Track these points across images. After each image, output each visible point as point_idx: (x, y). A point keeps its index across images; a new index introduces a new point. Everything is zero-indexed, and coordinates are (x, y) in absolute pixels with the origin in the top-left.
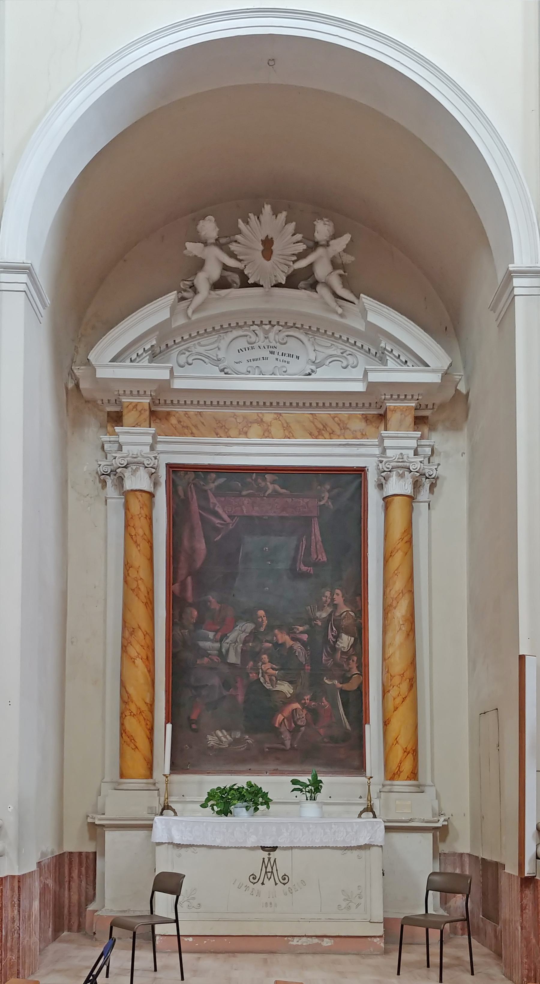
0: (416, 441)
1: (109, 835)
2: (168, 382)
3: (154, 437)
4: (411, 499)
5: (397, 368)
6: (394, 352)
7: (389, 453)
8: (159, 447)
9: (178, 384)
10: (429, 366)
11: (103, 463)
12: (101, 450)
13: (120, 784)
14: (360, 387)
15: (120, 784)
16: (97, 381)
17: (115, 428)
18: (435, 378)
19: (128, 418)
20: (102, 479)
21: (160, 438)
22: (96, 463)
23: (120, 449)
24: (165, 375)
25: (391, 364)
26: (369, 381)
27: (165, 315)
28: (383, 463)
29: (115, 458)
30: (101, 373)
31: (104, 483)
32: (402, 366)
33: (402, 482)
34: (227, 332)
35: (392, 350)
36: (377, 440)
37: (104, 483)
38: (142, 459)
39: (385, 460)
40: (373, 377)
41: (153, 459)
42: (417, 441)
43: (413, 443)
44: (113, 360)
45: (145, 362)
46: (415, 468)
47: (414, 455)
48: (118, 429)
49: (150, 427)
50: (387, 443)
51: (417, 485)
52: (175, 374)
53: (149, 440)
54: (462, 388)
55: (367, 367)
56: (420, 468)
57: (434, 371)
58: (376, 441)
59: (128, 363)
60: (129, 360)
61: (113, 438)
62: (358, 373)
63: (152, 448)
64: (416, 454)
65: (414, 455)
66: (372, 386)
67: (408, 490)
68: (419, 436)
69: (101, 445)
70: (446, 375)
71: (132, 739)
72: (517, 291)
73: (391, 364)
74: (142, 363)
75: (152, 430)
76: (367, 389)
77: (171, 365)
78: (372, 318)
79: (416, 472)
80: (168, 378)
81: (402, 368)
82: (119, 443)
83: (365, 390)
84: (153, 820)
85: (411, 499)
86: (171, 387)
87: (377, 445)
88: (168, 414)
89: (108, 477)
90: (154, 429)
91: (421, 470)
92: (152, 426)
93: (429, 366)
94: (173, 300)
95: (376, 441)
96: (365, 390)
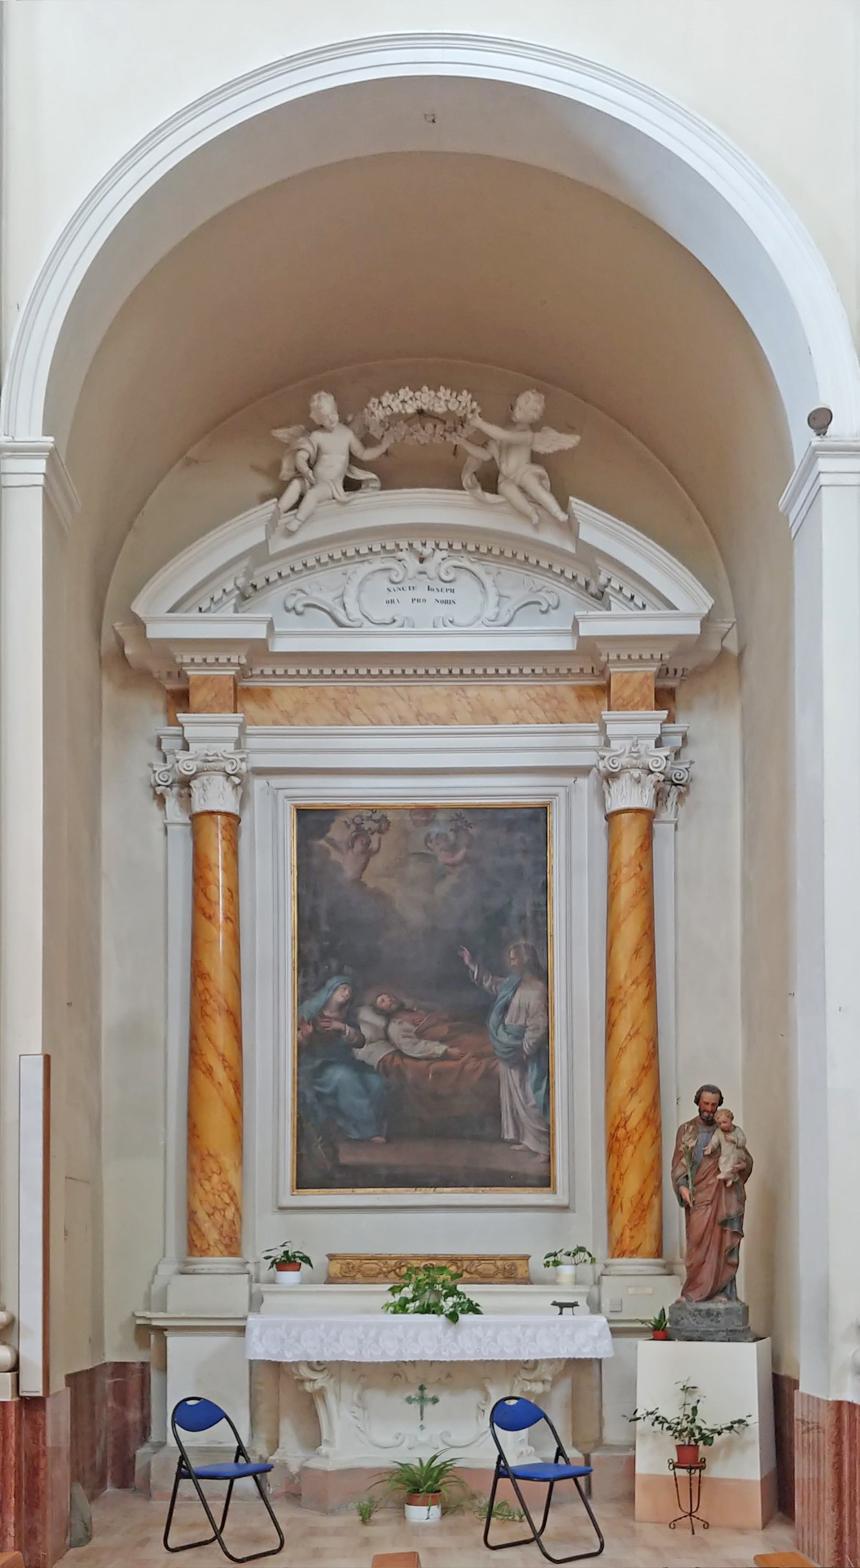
0: (659, 725)
1: (173, 1342)
2: (264, 642)
3: (242, 728)
4: (648, 816)
5: (624, 613)
6: (624, 591)
7: (614, 744)
8: (252, 743)
9: (281, 645)
10: (677, 609)
11: (159, 770)
12: (155, 749)
13: (187, 1264)
14: (567, 644)
15: (187, 1264)
16: (148, 642)
17: (178, 715)
18: (693, 628)
19: (196, 699)
20: (158, 793)
21: (250, 729)
22: (150, 769)
23: (186, 747)
24: (259, 632)
25: (617, 608)
26: (581, 634)
27: (258, 536)
28: (606, 759)
29: (178, 762)
30: (154, 632)
31: (161, 800)
32: (600, 610)
33: (637, 790)
34: (364, 561)
35: (621, 589)
36: (597, 725)
37: (161, 800)
38: (222, 765)
39: (608, 755)
40: (585, 630)
41: (239, 761)
42: (661, 724)
43: (655, 729)
44: (171, 611)
45: (228, 611)
46: (233, 768)
47: (656, 747)
48: (182, 717)
49: (236, 712)
50: (611, 729)
51: (660, 797)
52: (276, 629)
53: (234, 732)
54: (732, 645)
55: (577, 613)
56: (665, 768)
57: (689, 616)
58: (595, 727)
59: (195, 614)
60: (198, 609)
61: (175, 730)
62: (560, 621)
63: (238, 744)
64: (659, 744)
65: (656, 747)
66: (583, 641)
67: (644, 799)
68: (665, 717)
69: (156, 740)
70: (706, 621)
71: (227, 1067)
72: (824, 479)
73: (617, 608)
74: (222, 612)
75: (239, 717)
76: (577, 648)
77: (270, 615)
78: (586, 534)
79: (660, 772)
80: (264, 636)
81: (632, 612)
82: (184, 738)
83: (575, 648)
84: (245, 1319)
85: (648, 816)
86: (270, 650)
87: (597, 732)
88: (267, 692)
89: (169, 789)
90: (242, 715)
91: (667, 770)
92: (238, 711)
93: (677, 609)
94: (270, 515)
95: (595, 727)
96: (575, 648)
